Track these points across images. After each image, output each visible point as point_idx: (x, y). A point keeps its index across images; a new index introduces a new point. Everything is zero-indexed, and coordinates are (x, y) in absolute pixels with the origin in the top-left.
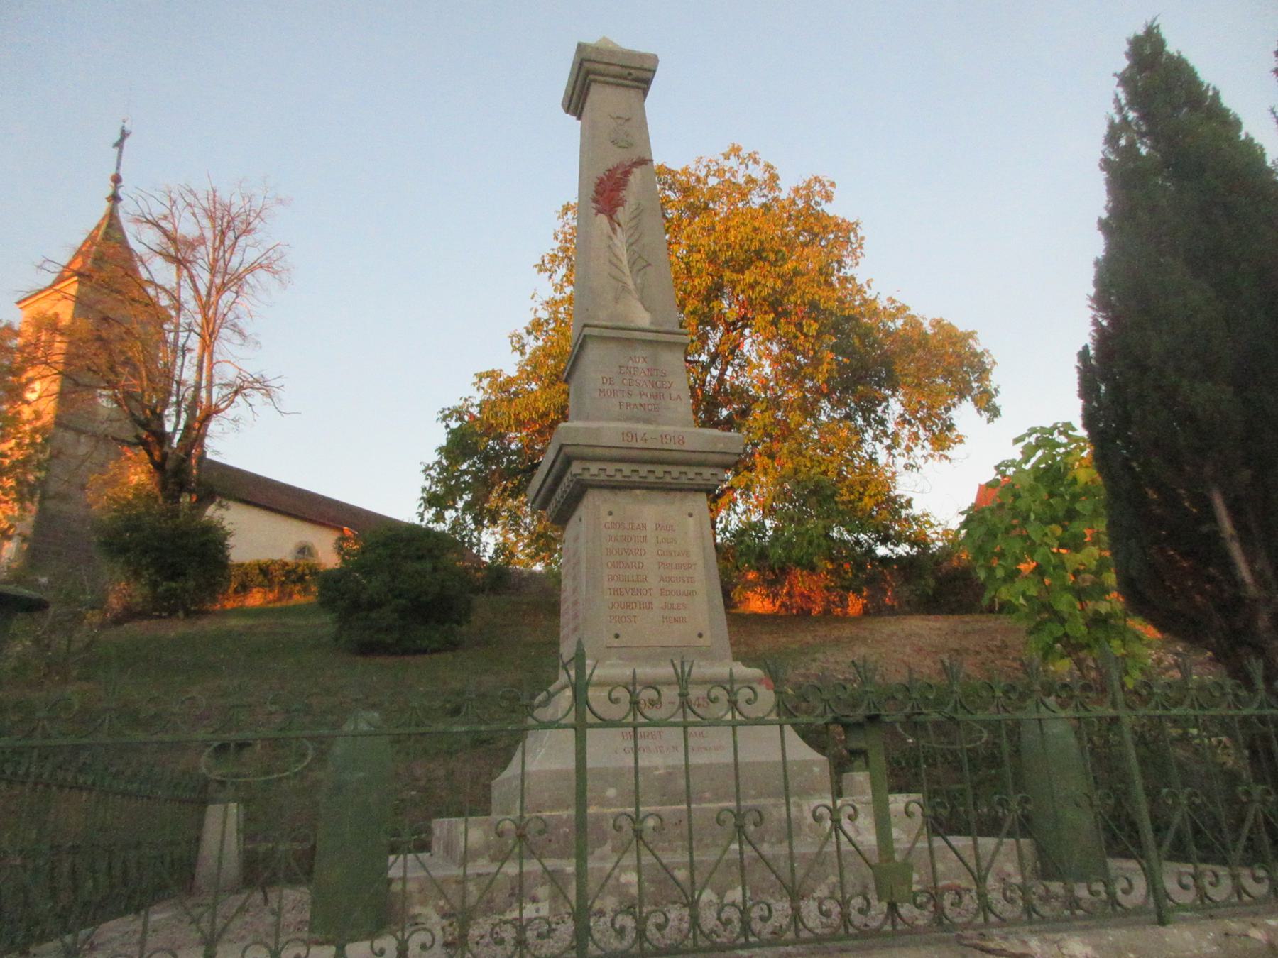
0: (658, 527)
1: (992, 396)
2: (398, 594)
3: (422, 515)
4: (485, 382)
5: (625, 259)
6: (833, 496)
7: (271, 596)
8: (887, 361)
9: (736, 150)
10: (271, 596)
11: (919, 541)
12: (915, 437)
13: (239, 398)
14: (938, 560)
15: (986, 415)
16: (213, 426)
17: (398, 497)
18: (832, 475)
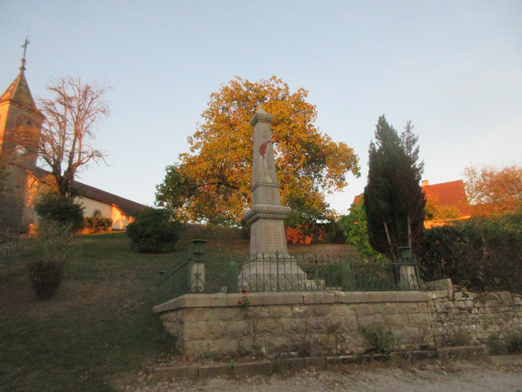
0: (274, 227)
1: (358, 170)
2: (151, 232)
3: (155, 203)
4: (183, 157)
5: (266, 166)
6: (303, 203)
7: (92, 231)
8: (324, 156)
9: (274, 78)
10: (92, 231)
11: (331, 219)
12: (331, 183)
13: (91, 158)
14: (336, 225)
15: (356, 176)
16: (79, 168)
17: (147, 197)
18: (303, 196)
